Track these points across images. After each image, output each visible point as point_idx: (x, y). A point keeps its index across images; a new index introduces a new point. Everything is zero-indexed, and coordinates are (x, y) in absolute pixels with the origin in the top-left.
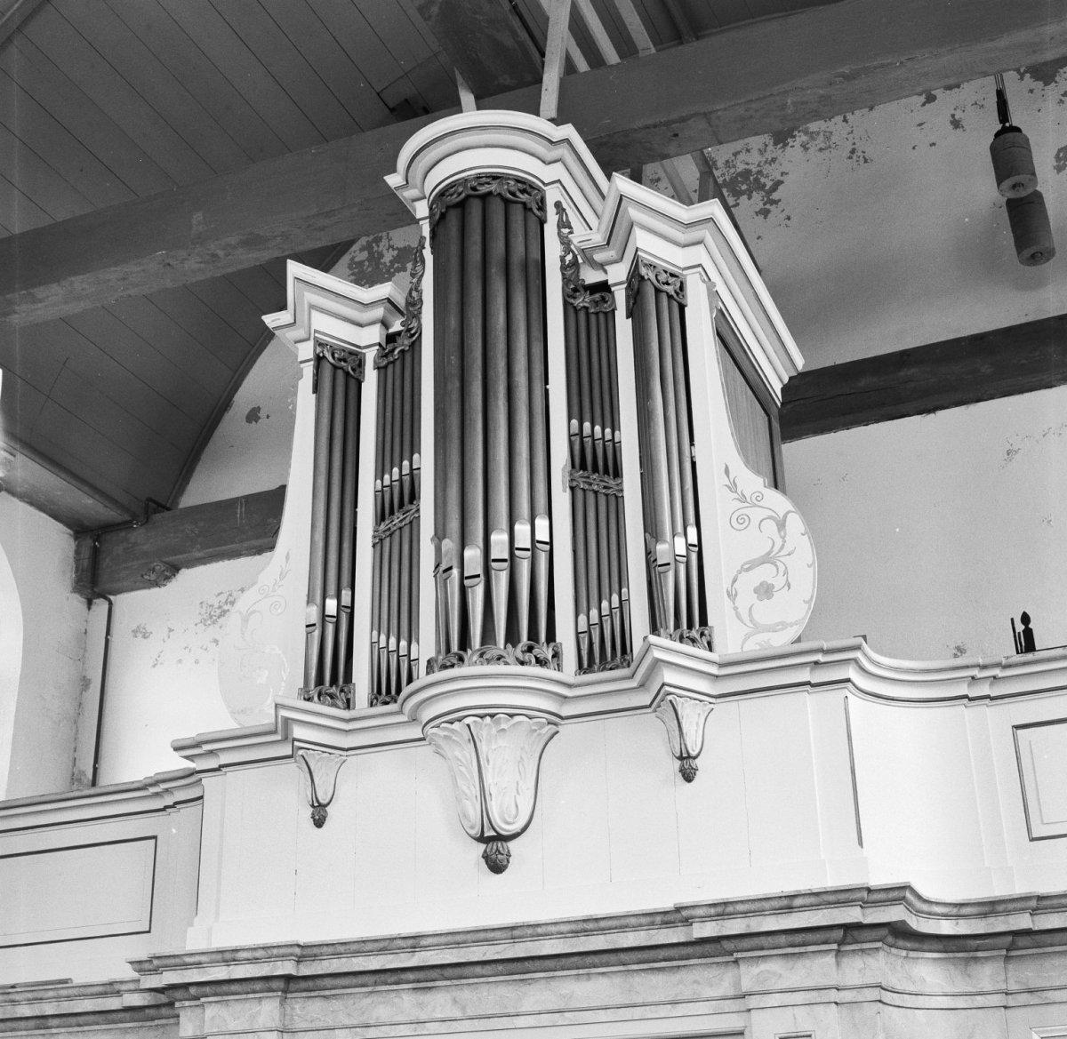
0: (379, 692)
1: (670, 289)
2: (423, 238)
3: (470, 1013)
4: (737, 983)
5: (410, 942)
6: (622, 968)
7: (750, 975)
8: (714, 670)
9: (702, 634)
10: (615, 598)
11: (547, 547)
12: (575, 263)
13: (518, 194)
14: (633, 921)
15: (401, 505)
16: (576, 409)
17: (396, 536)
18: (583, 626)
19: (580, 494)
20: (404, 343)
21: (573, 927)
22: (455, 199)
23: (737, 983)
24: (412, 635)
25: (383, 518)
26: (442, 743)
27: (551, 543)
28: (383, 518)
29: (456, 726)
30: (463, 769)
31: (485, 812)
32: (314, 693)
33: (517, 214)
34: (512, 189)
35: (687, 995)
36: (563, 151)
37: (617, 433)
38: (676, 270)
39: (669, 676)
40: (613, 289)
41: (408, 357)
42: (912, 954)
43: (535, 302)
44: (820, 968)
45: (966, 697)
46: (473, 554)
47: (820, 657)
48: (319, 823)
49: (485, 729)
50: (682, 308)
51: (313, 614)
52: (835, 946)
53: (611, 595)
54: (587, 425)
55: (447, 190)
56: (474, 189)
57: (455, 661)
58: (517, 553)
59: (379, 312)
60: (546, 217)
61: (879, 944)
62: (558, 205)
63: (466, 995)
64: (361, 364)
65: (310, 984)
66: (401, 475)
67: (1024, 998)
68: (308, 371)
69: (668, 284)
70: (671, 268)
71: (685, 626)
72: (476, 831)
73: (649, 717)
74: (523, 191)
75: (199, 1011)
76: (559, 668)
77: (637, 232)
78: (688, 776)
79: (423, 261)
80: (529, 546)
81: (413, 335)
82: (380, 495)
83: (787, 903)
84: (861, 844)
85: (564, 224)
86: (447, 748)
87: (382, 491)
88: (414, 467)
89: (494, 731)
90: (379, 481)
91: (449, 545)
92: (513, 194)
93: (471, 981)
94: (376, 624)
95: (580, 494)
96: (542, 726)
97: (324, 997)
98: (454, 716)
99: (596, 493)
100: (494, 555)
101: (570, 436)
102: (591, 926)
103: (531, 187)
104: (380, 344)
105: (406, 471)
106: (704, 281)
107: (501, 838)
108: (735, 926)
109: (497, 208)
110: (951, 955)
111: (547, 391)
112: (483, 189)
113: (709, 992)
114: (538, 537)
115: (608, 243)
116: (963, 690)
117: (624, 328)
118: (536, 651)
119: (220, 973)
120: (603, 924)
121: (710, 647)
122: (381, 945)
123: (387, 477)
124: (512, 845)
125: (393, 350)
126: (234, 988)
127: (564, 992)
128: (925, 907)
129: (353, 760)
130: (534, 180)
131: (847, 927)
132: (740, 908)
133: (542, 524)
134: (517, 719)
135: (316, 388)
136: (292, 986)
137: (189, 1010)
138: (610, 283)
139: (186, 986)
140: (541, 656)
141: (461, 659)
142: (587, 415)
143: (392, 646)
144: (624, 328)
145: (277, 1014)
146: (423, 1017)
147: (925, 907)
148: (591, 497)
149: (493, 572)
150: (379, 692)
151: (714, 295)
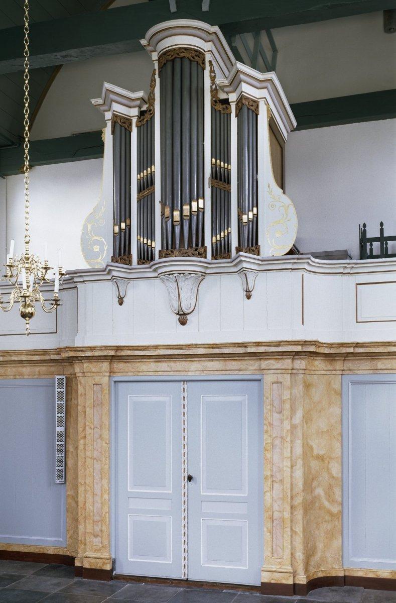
0: (141, 258)
1: (253, 108)
2: (155, 70)
3: (173, 369)
4: (260, 366)
5: (155, 347)
6: (223, 358)
7: (264, 364)
8: (260, 262)
9: (256, 248)
10: (226, 231)
11: (203, 210)
12: (216, 89)
13: (195, 57)
14: (229, 345)
15: (147, 186)
16: (214, 155)
17: (146, 199)
18: (214, 241)
19: (214, 189)
20: (147, 117)
21: (209, 346)
22: (170, 58)
23: (260, 366)
24: (152, 237)
25: (140, 191)
26: (165, 281)
27: (204, 209)
28: (140, 191)
29: (171, 276)
30: (172, 290)
31: (180, 305)
32: (119, 259)
33: (194, 64)
34: (193, 55)
35: (243, 367)
36: (213, 37)
37: (229, 166)
38: (255, 99)
39: (245, 265)
40: (231, 104)
41: (149, 122)
42: (315, 358)
43: (200, 110)
44: (287, 363)
45: (342, 273)
46: (177, 214)
47: (296, 261)
48: (121, 304)
49: (181, 278)
50: (257, 115)
51: (117, 229)
52: (292, 357)
53: (224, 230)
54: (218, 161)
55: (167, 53)
56: (178, 54)
57: (170, 253)
58: (192, 213)
59: (138, 102)
60: (205, 67)
61: (306, 357)
62: (210, 62)
63: (172, 364)
64: (131, 124)
65: (120, 358)
66: (147, 174)
67: (348, 372)
68: (109, 124)
69: (252, 106)
70: (254, 98)
71: (250, 246)
72: (176, 311)
73: (236, 276)
74: (197, 56)
75: (81, 364)
76: (205, 257)
77: (243, 84)
78: (249, 297)
79: (155, 81)
80: (196, 210)
81: (151, 114)
82: (139, 181)
83: (279, 344)
84: (303, 324)
85: (212, 71)
86: (168, 283)
87: (140, 180)
88: (153, 171)
89: (184, 279)
90: (139, 175)
91: (168, 211)
92: (193, 57)
93: (174, 359)
94: (139, 233)
95: (214, 189)
96: (200, 277)
97: (125, 362)
98: (170, 273)
99: (221, 189)
100: (185, 214)
101: (212, 165)
102: (214, 346)
103: (200, 53)
104: (138, 116)
105: (149, 172)
106: (266, 104)
107: (185, 314)
108: (261, 349)
109: (186, 63)
110: (327, 358)
111: (204, 145)
112: (182, 55)
113: (251, 368)
114: (200, 207)
115: (230, 85)
116: (341, 270)
117: (234, 121)
118: (198, 250)
119: (89, 354)
120: (218, 346)
121: (259, 254)
122: (145, 348)
123: (142, 174)
124: (188, 316)
125: (143, 120)
126: (94, 358)
127: (204, 365)
128: (321, 345)
129: (132, 282)
130: (201, 50)
131: (297, 352)
132: (263, 344)
133: (201, 201)
134: (192, 275)
135: (113, 133)
136: (114, 358)
137: (78, 364)
138: (230, 101)
139: (77, 357)
140: (200, 252)
141: (172, 252)
142: (218, 157)
143: (145, 242)
144: (234, 121)
145: (108, 367)
146: (158, 370)
147: (321, 345)
148: (218, 190)
149: (185, 221)
150: (141, 258)
151: (269, 110)
